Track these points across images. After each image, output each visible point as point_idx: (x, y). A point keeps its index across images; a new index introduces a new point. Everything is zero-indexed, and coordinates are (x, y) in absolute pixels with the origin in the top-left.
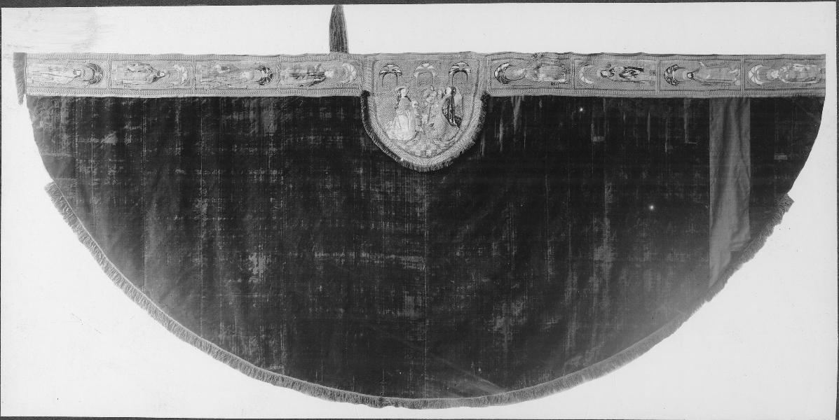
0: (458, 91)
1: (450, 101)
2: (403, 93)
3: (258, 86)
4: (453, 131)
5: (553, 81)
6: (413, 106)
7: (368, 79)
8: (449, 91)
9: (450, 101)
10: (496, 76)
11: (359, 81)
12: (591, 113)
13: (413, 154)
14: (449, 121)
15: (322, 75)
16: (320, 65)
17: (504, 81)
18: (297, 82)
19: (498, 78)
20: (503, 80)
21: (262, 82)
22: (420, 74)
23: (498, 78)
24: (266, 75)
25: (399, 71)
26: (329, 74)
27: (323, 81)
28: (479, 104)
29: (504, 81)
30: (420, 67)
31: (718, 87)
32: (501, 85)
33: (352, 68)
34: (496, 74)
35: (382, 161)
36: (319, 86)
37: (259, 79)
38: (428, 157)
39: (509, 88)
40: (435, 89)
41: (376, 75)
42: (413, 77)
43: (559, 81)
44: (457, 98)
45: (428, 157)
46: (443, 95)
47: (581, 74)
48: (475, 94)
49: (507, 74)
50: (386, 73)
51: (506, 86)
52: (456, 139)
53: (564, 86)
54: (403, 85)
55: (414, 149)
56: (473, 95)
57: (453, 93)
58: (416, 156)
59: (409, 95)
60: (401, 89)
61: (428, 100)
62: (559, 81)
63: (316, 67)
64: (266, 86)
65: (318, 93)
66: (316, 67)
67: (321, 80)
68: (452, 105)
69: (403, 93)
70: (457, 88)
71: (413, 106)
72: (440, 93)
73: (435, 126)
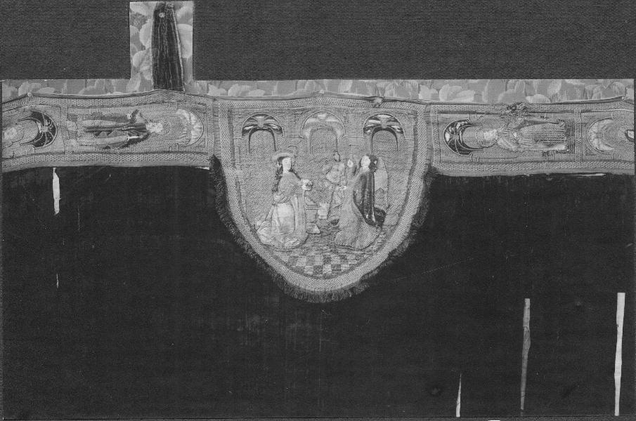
0: (381, 164)
1: (367, 182)
2: (286, 164)
3: (31, 149)
4: (369, 234)
5: (546, 150)
6: (304, 187)
7: (224, 139)
8: (366, 162)
9: (367, 182)
10: (448, 140)
11: (209, 139)
12: (329, 171)
13: (300, 271)
14: (364, 217)
15: (140, 129)
16: (136, 112)
17: (461, 148)
18: (99, 141)
19: (452, 145)
20: (459, 147)
21: (40, 141)
22: (313, 131)
23: (452, 145)
24: (45, 130)
25: (276, 127)
26: (155, 128)
27: (143, 140)
28: (418, 185)
29: (461, 148)
30: (311, 120)
31: (490, 161)
32: (455, 156)
33: (193, 118)
34: (448, 136)
35: (253, 276)
36: (140, 147)
37: (33, 136)
38: (326, 277)
39: (471, 162)
40: (342, 157)
41: (238, 135)
42: (302, 138)
43: (556, 148)
44: (380, 178)
45: (326, 277)
46: (355, 171)
47: (594, 135)
48: (411, 172)
49: (468, 136)
50: (255, 130)
51: (466, 158)
52: (375, 248)
53: (564, 156)
54: (285, 150)
55: (302, 262)
56: (407, 172)
57: (373, 167)
58: (307, 275)
59: (296, 168)
60: (281, 159)
61: (329, 176)
62: (556, 148)
63: (129, 116)
64: (47, 148)
65: (134, 160)
66: (129, 116)
67: (141, 137)
68: (370, 189)
69: (286, 164)
70: (380, 158)
71: (304, 187)
72: (351, 165)
73: (341, 224)
